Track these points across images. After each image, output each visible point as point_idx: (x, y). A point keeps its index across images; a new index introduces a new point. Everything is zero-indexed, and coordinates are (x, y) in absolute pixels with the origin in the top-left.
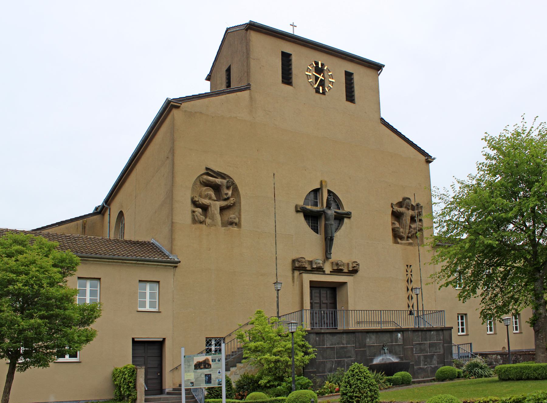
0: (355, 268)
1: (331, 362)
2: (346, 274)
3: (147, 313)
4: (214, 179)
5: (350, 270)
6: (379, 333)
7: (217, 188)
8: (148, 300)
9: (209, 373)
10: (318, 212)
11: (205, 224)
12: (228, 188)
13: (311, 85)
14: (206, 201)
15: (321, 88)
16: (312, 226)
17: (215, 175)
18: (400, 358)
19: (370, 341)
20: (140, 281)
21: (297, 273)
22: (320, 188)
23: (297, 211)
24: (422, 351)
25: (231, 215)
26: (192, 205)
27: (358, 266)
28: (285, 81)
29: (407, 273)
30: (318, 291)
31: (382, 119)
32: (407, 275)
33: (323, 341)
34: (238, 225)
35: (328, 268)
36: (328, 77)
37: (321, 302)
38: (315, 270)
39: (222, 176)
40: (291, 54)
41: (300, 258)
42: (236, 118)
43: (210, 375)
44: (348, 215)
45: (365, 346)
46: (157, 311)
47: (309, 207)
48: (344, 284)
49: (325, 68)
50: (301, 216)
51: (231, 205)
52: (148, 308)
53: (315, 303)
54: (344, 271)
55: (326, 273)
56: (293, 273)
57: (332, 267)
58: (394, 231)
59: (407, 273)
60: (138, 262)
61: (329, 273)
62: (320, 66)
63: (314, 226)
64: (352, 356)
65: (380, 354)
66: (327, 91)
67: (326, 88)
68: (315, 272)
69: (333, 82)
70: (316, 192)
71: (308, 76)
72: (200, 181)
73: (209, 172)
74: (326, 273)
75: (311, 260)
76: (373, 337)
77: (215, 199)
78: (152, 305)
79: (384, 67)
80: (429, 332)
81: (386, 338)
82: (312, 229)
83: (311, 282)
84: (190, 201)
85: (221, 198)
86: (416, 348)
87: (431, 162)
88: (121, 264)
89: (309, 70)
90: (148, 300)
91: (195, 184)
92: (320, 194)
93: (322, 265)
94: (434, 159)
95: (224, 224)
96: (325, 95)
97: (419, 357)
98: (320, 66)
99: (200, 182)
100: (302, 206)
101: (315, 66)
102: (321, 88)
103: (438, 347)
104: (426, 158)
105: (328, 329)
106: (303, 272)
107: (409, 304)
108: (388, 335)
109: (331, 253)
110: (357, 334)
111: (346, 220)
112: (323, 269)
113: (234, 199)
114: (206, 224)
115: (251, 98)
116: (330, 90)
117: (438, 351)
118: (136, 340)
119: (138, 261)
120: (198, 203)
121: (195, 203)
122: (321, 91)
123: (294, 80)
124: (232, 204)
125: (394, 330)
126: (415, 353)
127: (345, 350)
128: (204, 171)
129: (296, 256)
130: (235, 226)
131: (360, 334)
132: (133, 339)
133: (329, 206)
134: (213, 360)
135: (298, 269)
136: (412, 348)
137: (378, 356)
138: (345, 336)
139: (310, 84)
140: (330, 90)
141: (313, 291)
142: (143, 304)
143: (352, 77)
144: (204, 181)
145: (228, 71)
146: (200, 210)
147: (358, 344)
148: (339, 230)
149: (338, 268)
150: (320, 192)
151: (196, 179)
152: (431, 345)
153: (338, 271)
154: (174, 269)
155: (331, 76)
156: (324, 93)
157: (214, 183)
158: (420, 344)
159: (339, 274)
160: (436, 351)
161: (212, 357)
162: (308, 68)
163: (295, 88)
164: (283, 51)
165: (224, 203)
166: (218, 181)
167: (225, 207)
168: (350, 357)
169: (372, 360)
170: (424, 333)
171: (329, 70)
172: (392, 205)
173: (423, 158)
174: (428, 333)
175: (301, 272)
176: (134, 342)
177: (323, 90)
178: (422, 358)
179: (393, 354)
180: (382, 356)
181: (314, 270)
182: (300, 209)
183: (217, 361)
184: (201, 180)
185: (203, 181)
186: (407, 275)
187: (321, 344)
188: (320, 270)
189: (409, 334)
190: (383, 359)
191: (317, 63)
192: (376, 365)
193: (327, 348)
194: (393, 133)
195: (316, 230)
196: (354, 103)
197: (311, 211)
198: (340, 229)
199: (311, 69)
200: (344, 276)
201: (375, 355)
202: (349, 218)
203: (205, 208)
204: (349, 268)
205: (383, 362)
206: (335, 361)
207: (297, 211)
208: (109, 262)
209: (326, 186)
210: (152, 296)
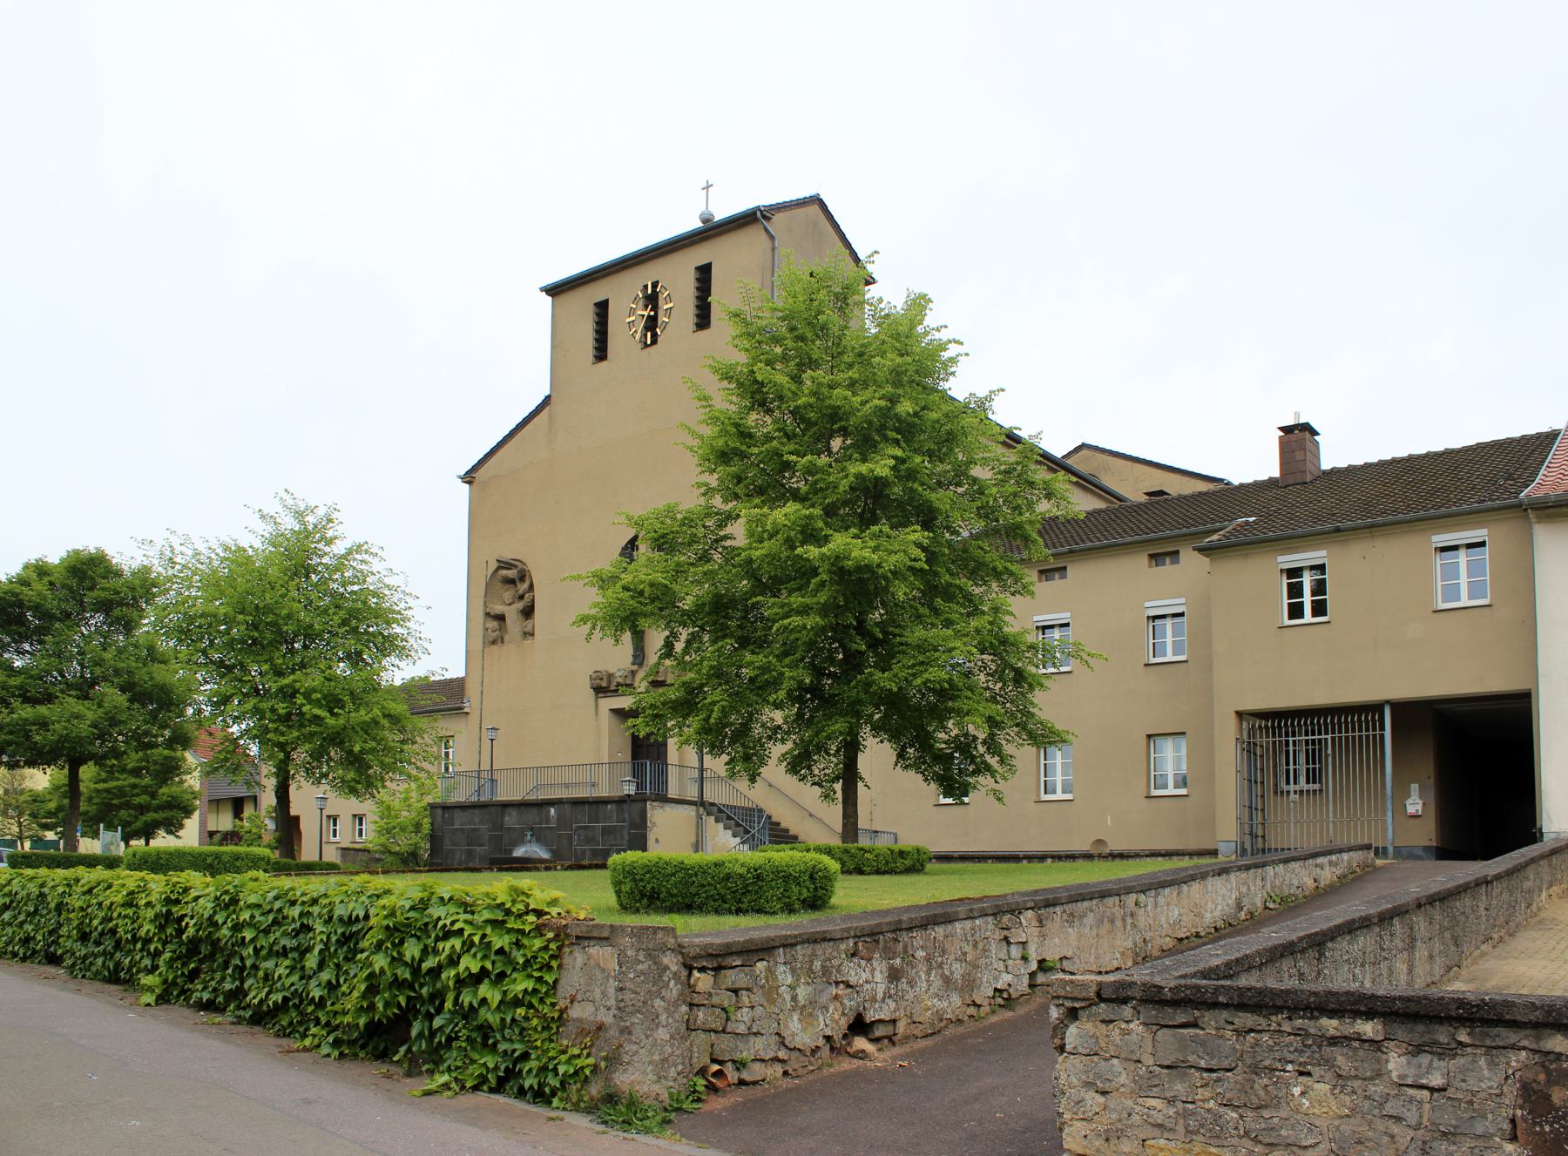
6: (523, 808)
8: (1464, 581)
14: (498, 608)
15: (649, 334)
18: (552, 851)
19: (511, 820)
24: (590, 840)
33: (453, 818)
45: (501, 827)
73: (504, 565)
76: (514, 812)
80: (604, 806)
81: (531, 815)
86: (580, 836)
90: (1464, 581)
97: (583, 852)
102: (649, 334)
108: (535, 810)
115: (551, 419)
117: (619, 842)
122: (649, 342)
126: (577, 845)
128: (496, 565)
131: (494, 808)
136: (570, 837)
138: (477, 811)
142: (1452, 592)
152: (606, 831)
158: (585, 828)
160: (613, 843)
164: (610, 302)
168: (482, 845)
169: (511, 851)
170: (594, 806)
174: (601, 807)
176: (1240, 715)
178: (588, 852)
188: (627, 686)
190: (526, 851)
191: (646, 287)
192: (515, 858)
203: (501, 618)
205: (527, 856)
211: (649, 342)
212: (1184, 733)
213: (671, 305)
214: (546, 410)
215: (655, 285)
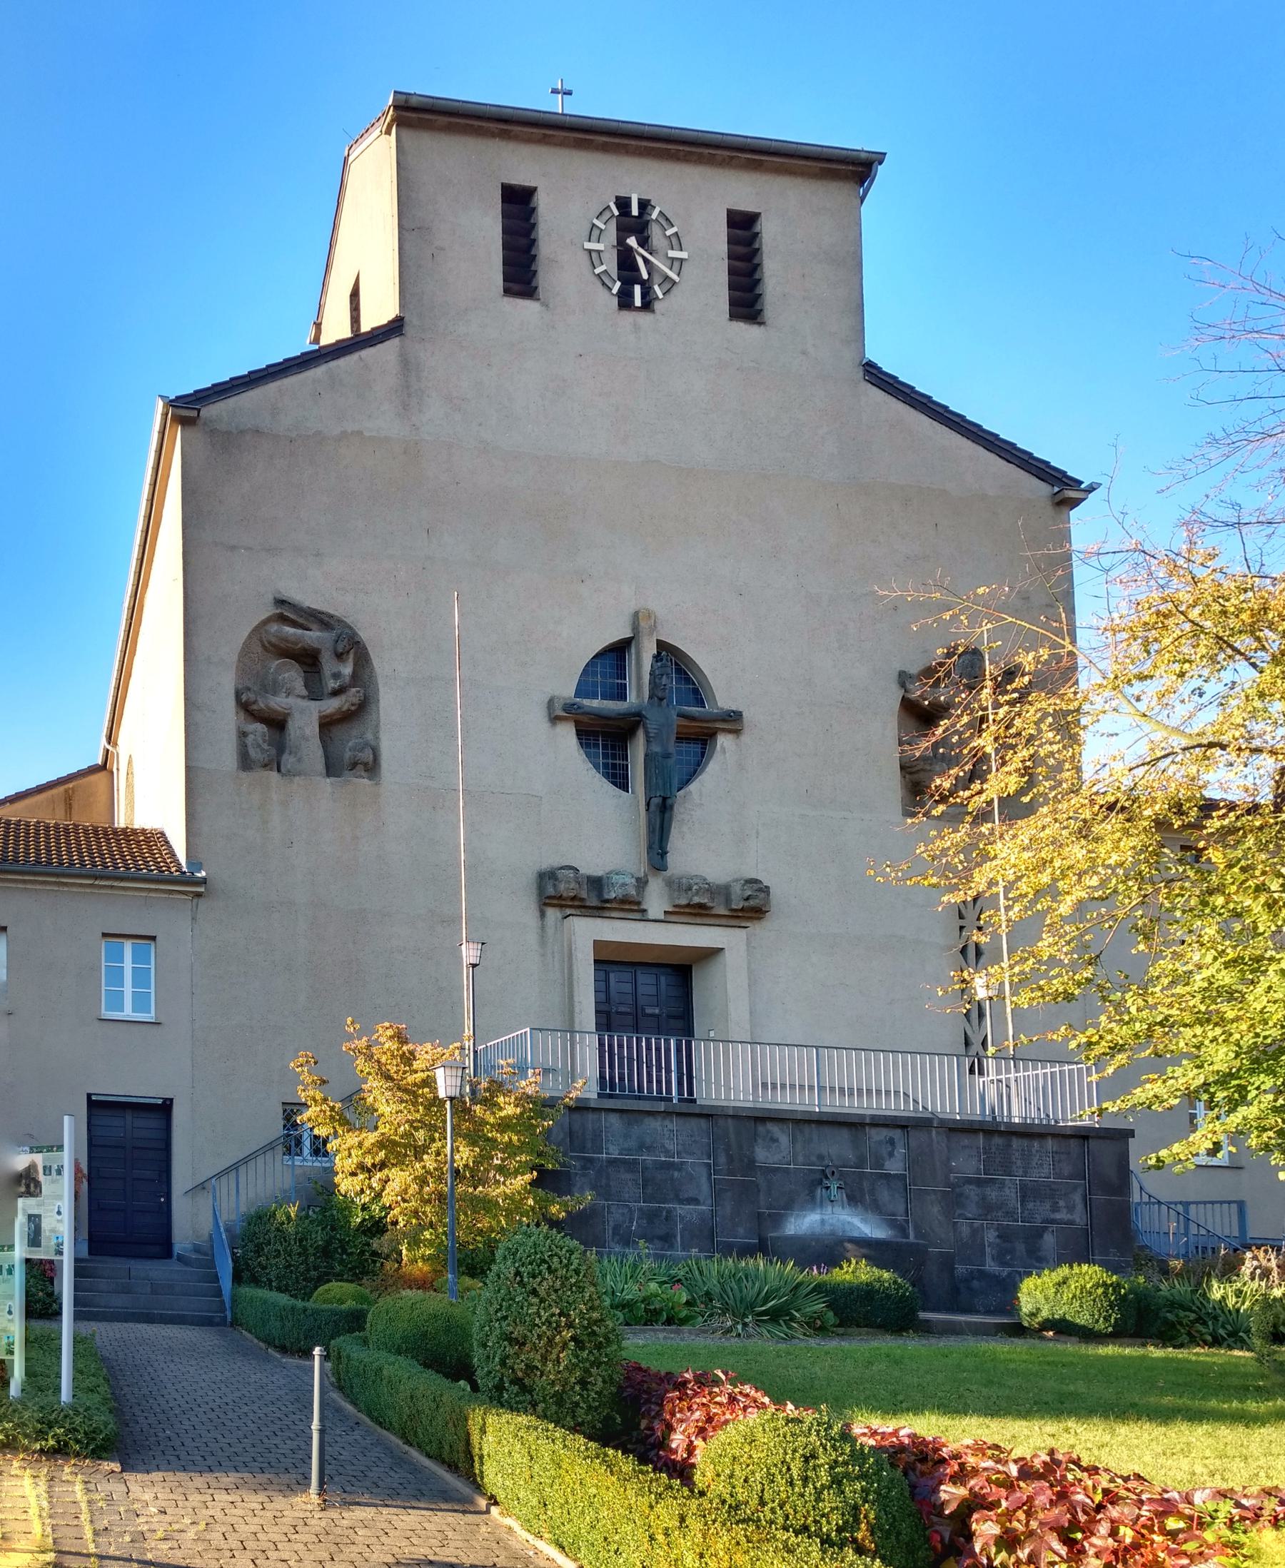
0: (752, 903)
1: (626, 1211)
2: (723, 921)
3: (124, 1026)
4: (300, 631)
5: (734, 907)
7: (308, 660)
8: (128, 989)
9: (35, 1212)
10: (624, 716)
11: (279, 770)
12: (340, 656)
13: (604, 284)
16: (606, 766)
17: (301, 620)
18: (892, 1224)
20: (105, 935)
21: (553, 914)
22: (633, 638)
23: (554, 720)
25: (349, 740)
26: (242, 714)
27: (762, 895)
28: (516, 287)
29: (962, 923)
30: (627, 976)
31: (875, 375)
32: (962, 928)
34: (371, 768)
35: (656, 902)
36: (665, 243)
37: (639, 1011)
38: (614, 905)
39: (322, 620)
40: (535, 189)
41: (562, 868)
42: (360, 433)
43: (39, 1216)
44: (733, 722)
46: (153, 1021)
47: (595, 704)
48: (711, 954)
49: (654, 216)
50: (567, 734)
51: (353, 708)
52: (128, 1012)
53: (617, 1013)
54: (714, 912)
55: (651, 915)
56: (542, 915)
57: (671, 898)
58: (911, 773)
59: (962, 923)
60: (96, 883)
61: (662, 917)
62: (635, 212)
63: (614, 766)
64: (701, 1199)
65: (812, 1202)
66: (661, 296)
67: (656, 288)
68: (614, 914)
69: (682, 260)
70: (618, 652)
71: (594, 255)
72: (261, 641)
73: (286, 611)
74: (651, 915)
75: (598, 872)
77: (305, 692)
78: (140, 1002)
79: (881, 163)
82: (606, 775)
83: (598, 945)
84: (231, 703)
85: (326, 691)
87: (1075, 503)
88: (56, 888)
89: (596, 232)
90: (128, 989)
91: (245, 651)
92: (633, 657)
93: (634, 892)
94: (1091, 489)
95: (332, 768)
96: (653, 311)
98: (635, 212)
99: (263, 646)
100: (570, 698)
101: (616, 213)
103: (1062, 1203)
104: (1056, 489)
105: (611, 1096)
106: (574, 912)
107: (969, 1033)
109: (666, 853)
110: (721, 1122)
111: (723, 741)
112: (639, 903)
113: (358, 692)
114: (283, 769)
115: (406, 364)
116: (668, 291)
118: (94, 1098)
119: (96, 878)
120: (255, 707)
121: (246, 707)
122: (638, 302)
123: (546, 278)
124: (352, 705)
125: (868, 1121)
127: (676, 1174)
128: (271, 611)
129: (551, 860)
130: (363, 774)
132: (89, 1096)
133: (658, 694)
134: (47, 1170)
135: (555, 902)
137: (803, 1208)
139: (599, 284)
140: (668, 291)
141: (612, 975)
143: (757, 229)
144: (273, 640)
145: (355, 295)
146: (260, 728)
147: (722, 1159)
148: (700, 774)
149: (691, 900)
150: (633, 650)
151: (250, 637)
153: (696, 912)
154: (195, 901)
155: (674, 240)
156: (647, 305)
157: (300, 646)
159: (698, 920)
161: (44, 1160)
162: (594, 225)
163: (546, 305)
165: (332, 705)
166: (313, 636)
167: (335, 717)
168: (695, 1201)
171: (667, 219)
172: (904, 679)
173: (1044, 489)
175: (568, 911)
177: (644, 296)
179: (866, 1209)
180: (819, 1211)
181: (608, 905)
182: (565, 710)
183: (54, 1172)
184: (264, 639)
185: (269, 642)
186: (962, 928)
187: (589, 1145)
188: (631, 907)
189: (930, 1137)
191: (623, 204)
193: (612, 1162)
194: (912, 410)
195: (619, 779)
196: (761, 324)
197: (599, 716)
198: (703, 770)
199: (603, 227)
200: (712, 928)
201: (789, 1205)
202: (737, 732)
204: (731, 900)
206: (640, 1209)
207: (554, 720)
208: (24, 882)
209: (653, 628)
210: (140, 977)
211: (638, 302)
212: (153, 938)
213: (683, 255)
214: (393, 344)
215: (644, 205)
